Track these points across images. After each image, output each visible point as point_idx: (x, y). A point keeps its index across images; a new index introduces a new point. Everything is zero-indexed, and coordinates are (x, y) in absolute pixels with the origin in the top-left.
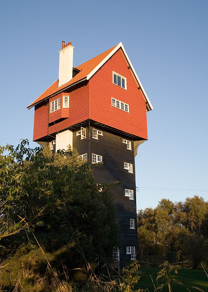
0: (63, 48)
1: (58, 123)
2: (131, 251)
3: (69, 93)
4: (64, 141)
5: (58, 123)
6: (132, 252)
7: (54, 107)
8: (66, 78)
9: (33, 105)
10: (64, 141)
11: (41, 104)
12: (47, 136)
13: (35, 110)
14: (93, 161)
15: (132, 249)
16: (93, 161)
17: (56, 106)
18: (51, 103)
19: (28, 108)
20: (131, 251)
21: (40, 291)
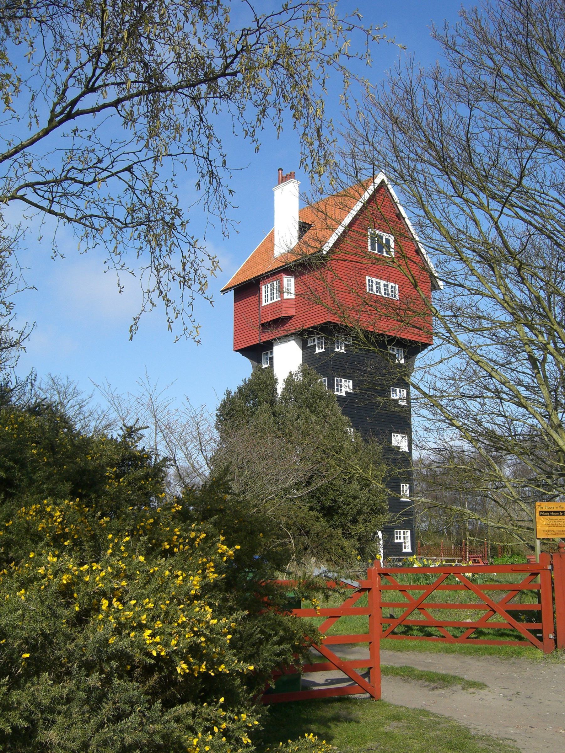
0: (279, 184)
1: (278, 325)
2: (402, 538)
3: (343, 414)
4: (287, 359)
5: (278, 325)
6: (404, 538)
7: (268, 296)
8: (285, 237)
9: (231, 288)
10: (287, 359)
11: (246, 290)
12: (259, 344)
13: (236, 301)
14: (337, 389)
15: (404, 534)
16: (337, 389)
17: (272, 294)
18: (263, 287)
19: (222, 291)
20: (402, 538)
21: (3, 397)
